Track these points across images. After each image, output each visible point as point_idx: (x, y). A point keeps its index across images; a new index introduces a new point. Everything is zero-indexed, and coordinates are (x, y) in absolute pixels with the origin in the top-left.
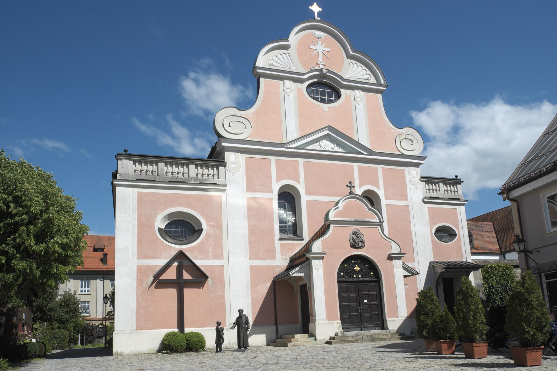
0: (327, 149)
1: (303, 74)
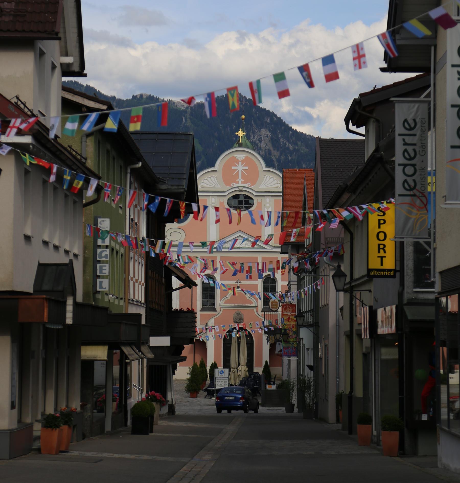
1: (224, 192)
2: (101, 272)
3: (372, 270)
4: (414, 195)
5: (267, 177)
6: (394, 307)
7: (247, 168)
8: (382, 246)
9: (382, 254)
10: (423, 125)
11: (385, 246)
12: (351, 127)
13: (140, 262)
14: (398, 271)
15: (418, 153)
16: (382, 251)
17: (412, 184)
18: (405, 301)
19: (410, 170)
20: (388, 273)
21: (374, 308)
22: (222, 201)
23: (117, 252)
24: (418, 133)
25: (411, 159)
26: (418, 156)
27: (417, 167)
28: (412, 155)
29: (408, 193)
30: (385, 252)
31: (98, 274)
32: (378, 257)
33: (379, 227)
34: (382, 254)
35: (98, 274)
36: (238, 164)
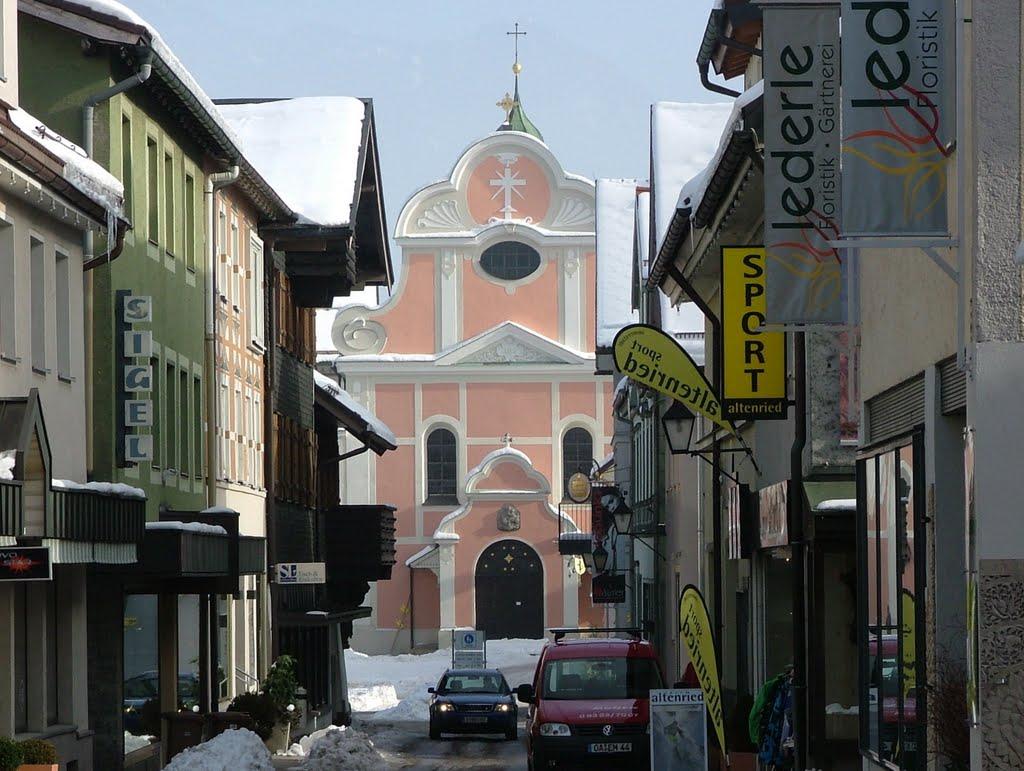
2: (134, 418)
3: (733, 402)
4: (810, 225)
6: (785, 485)
7: (522, 182)
8: (754, 347)
9: (755, 363)
10: (827, 61)
11: (761, 346)
12: (715, 78)
13: (250, 396)
14: (792, 403)
15: (815, 126)
16: (754, 357)
17: (804, 199)
18: (804, 474)
19: (797, 167)
20: (769, 409)
21: (752, 489)
23: (170, 368)
24: (818, 80)
25: (802, 140)
26: (817, 133)
27: (815, 160)
28: (804, 132)
29: (794, 219)
30: (761, 360)
31: (128, 423)
32: (746, 371)
33: (748, 303)
34: (755, 363)
35: (128, 423)
36: (517, 178)
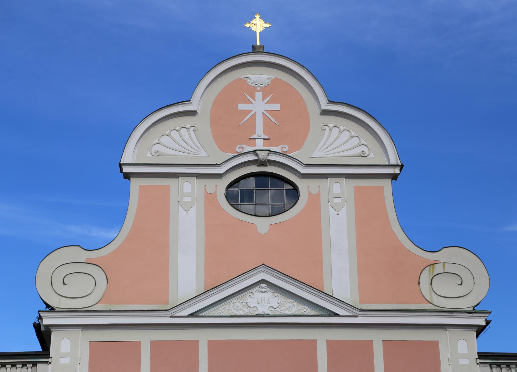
0: (260, 311)
5: (331, 130)
7: (277, 107)
22: (210, 190)
